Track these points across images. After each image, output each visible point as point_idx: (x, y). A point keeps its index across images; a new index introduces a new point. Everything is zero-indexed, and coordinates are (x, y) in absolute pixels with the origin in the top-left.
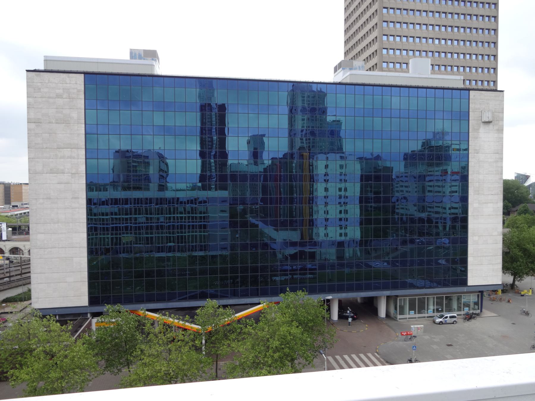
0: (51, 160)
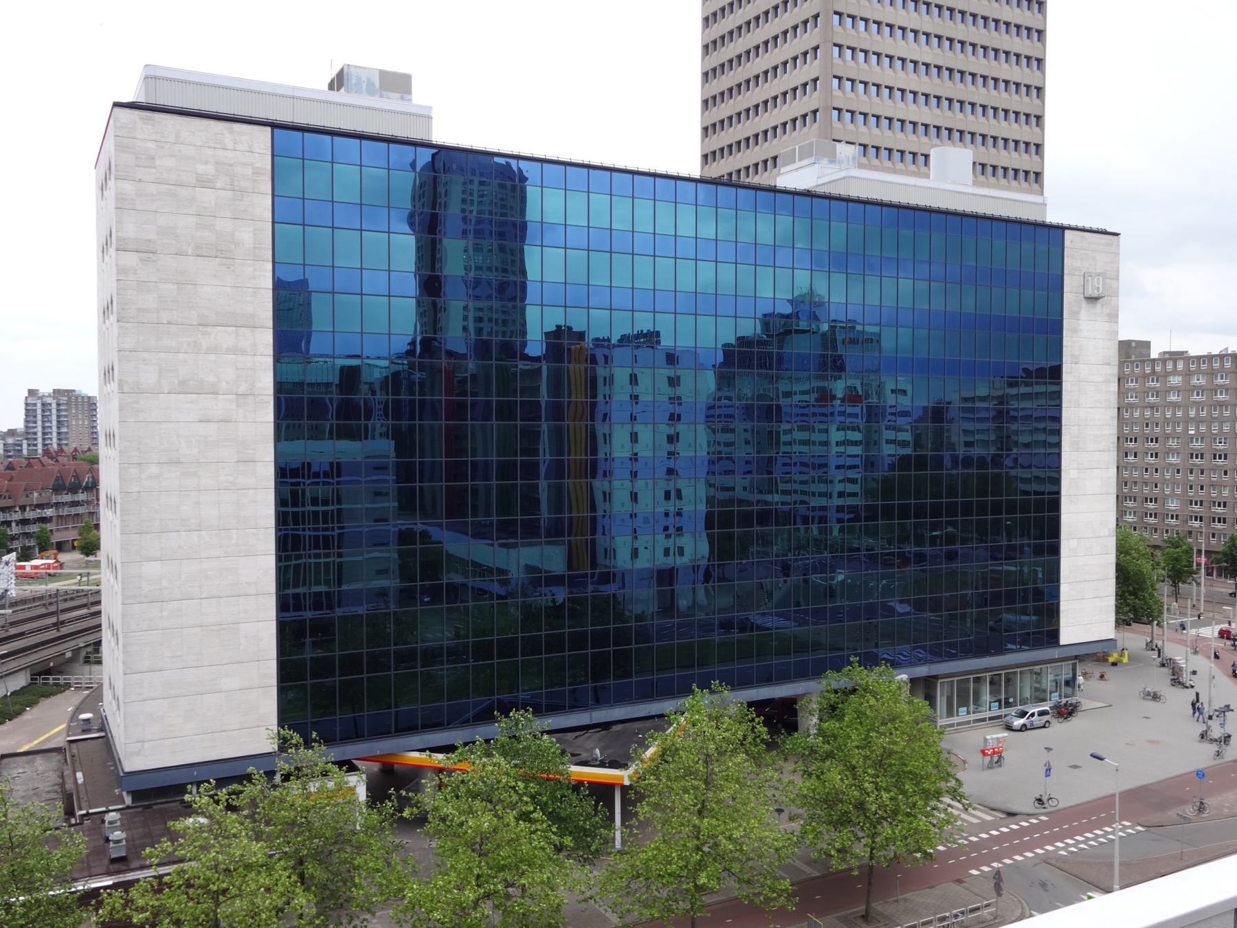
0: (181, 356)
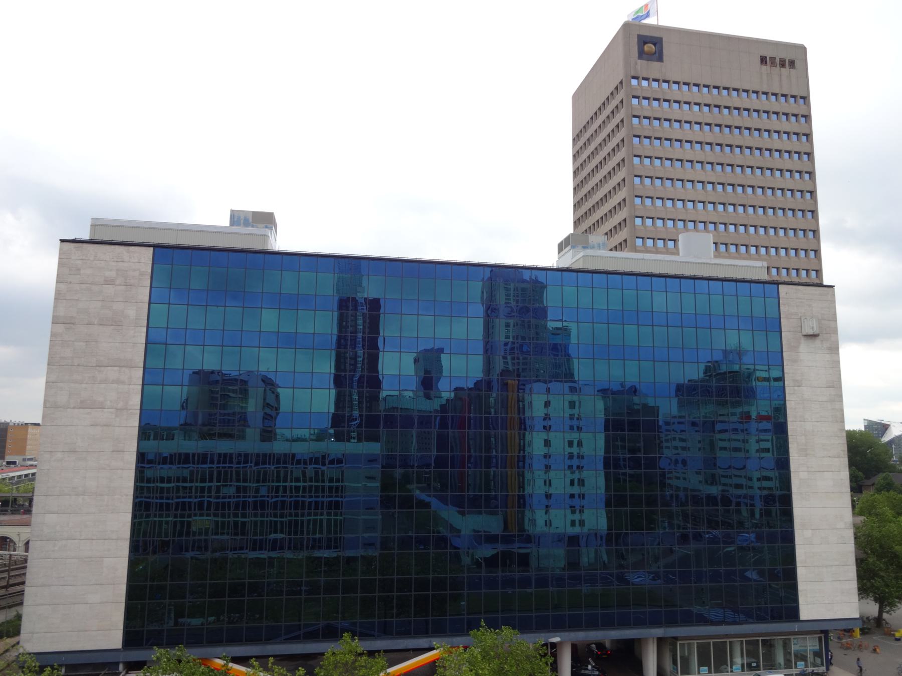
0: (84, 385)
